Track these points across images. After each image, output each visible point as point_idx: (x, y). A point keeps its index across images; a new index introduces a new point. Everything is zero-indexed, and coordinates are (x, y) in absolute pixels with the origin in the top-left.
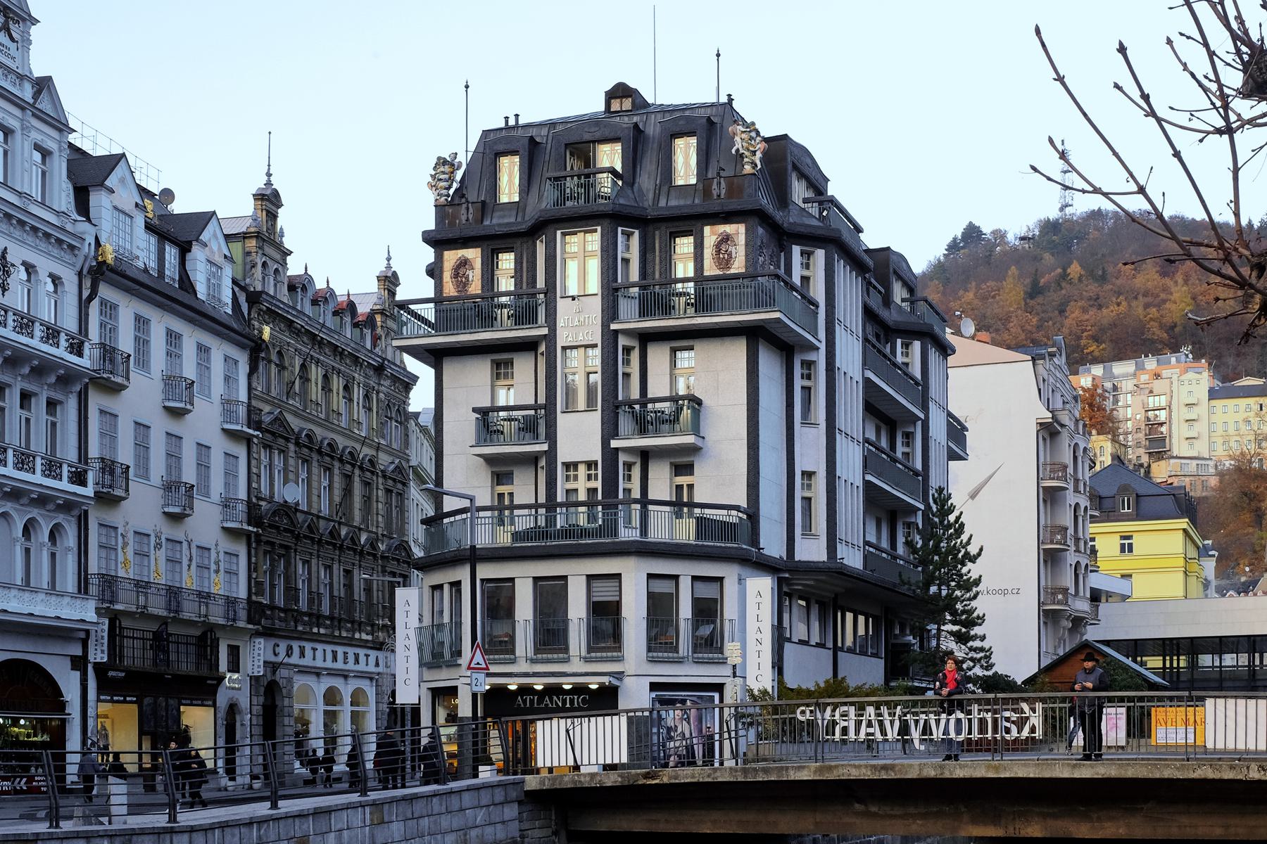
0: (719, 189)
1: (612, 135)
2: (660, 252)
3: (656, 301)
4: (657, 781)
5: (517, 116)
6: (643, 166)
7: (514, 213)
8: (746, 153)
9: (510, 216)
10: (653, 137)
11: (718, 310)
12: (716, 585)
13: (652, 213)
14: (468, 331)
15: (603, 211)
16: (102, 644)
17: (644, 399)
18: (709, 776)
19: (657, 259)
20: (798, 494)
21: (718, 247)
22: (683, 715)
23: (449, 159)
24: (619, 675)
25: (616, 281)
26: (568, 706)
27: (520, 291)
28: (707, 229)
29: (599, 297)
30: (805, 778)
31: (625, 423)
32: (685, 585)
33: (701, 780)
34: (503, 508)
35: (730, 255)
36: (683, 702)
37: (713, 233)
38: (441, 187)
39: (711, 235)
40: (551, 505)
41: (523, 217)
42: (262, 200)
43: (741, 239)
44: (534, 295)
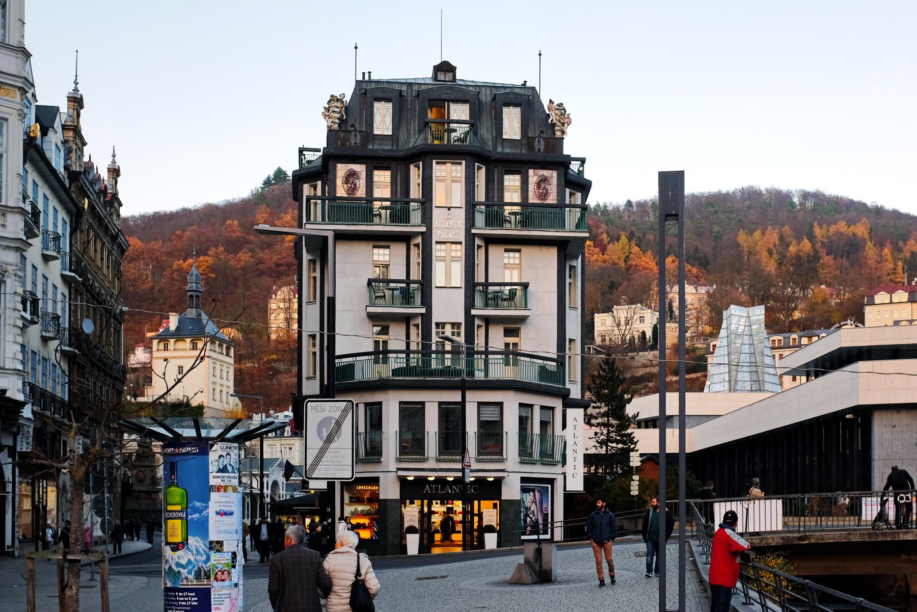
1: (463, 98)
3: (495, 218)
4: (807, 542)
5: (370, 73)
6: (482, 122)
7: (390, 143)
8: (558, 124)
9: (387, 145)
10: (486, 103)
13: (494, 156)
14: (365, 223)
16: (28, 438)
18: (845, 538)
19: (496, 187)
21: (539, 184)
28: (531, 172)
29: (463, 211)
30: (911, 539)
31: (478, 301)
32: (537, 410)
33: (840, 541)
34: (381, 353)
35: (547, 191)
36: (533, 491)
38: (335, 118)
39: (533, 176)
40: (426, 350)
41: (397, 146)
42: (74, 101)
43: (554, 181)
44: (408, 203)
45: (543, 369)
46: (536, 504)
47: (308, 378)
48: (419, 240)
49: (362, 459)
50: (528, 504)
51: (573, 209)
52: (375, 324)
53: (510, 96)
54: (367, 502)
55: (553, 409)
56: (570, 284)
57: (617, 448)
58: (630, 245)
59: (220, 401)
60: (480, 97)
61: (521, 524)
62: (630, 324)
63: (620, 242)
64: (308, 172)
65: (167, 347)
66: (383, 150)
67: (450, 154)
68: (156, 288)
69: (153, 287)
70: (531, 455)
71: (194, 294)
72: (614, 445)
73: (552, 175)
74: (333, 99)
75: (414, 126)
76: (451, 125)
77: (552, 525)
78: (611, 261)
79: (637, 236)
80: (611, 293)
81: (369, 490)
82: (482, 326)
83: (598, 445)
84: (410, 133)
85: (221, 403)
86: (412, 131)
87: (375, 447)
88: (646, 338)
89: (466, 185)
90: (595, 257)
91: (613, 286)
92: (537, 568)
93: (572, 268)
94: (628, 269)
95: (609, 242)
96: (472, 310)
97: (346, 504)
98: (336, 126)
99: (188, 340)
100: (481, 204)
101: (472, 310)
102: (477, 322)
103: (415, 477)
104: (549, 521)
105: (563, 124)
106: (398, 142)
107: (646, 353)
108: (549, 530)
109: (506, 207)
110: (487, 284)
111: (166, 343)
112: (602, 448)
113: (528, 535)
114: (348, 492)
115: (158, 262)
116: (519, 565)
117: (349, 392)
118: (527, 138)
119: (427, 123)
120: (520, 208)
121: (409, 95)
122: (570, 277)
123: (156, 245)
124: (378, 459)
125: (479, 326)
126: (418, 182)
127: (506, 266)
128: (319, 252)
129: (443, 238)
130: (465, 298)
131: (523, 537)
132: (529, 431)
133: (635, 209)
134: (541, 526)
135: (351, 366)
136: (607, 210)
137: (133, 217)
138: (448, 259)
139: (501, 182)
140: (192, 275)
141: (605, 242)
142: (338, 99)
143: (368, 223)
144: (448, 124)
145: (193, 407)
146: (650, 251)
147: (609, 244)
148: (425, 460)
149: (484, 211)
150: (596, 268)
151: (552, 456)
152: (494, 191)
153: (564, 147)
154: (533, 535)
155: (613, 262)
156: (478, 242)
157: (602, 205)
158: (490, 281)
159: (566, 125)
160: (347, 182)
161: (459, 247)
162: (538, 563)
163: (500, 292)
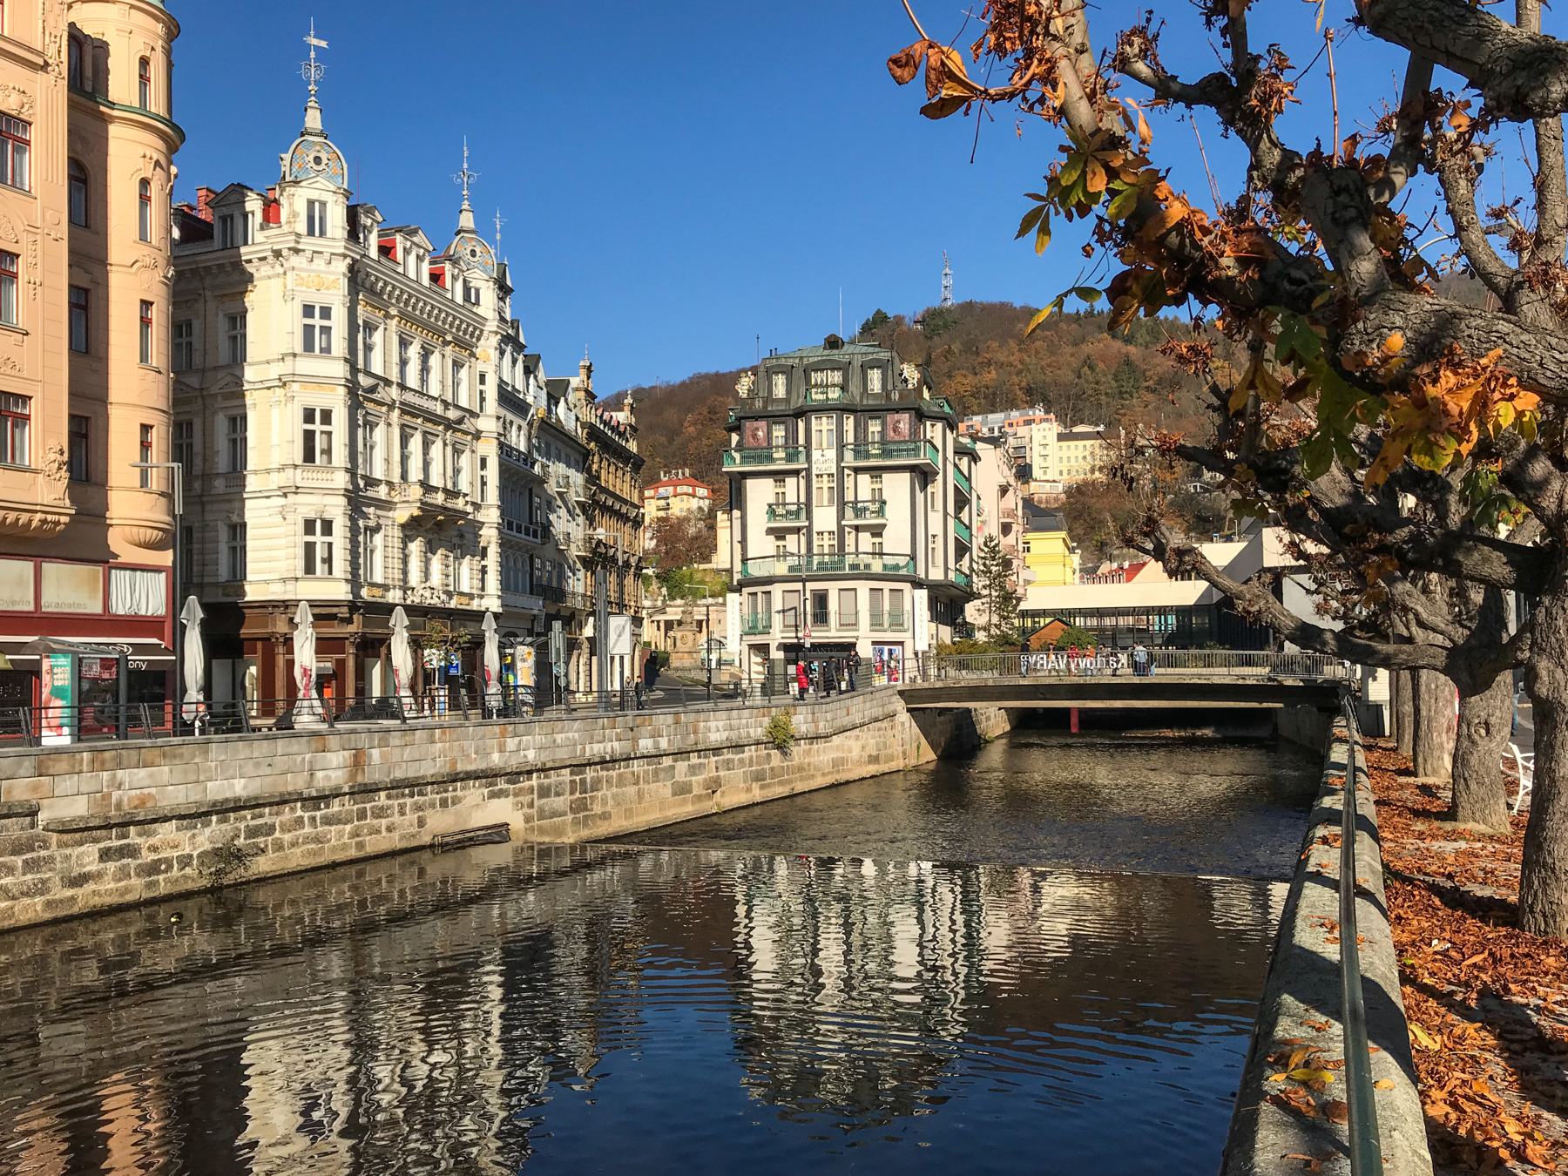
0: (896, 396)
17: (856, 502)
20: (930, 546)
24: (857, 638)
31: (849, 512)
32: (886, 593)
34: (782, 555)
67: (823, 409)
80: (1223, 397)
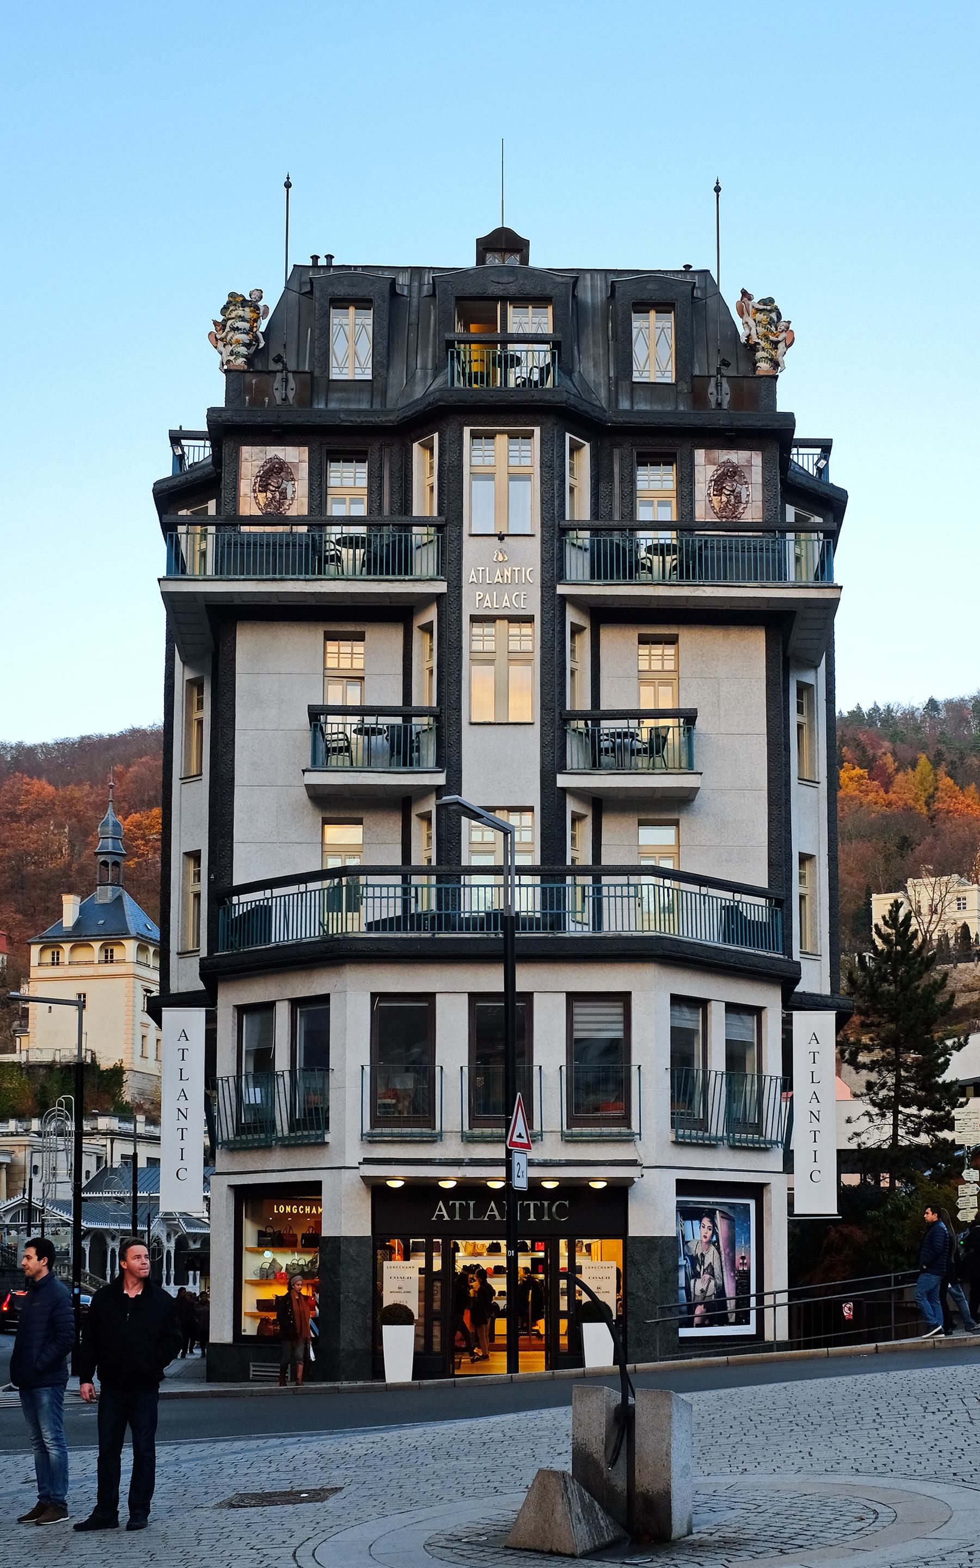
1: (537, 292)
2: (621, 482)
6: (582, 348)
8: (763, 344)
9: (359, 401)
11: (713, 578)
12: (752, 1021)
13: (611, 418)
14: (302, 577)
15: (550, 402)
19: (617, 491)
21: (718, 484)
22: (712, 1237)
23: (248, 298)
25: (564, 518)
26: (532, 1218)
27: (376, 519)
28: (700, 455)
29: (537, 541)
31: (575, 753)
32: (717, 1014)
36: (711, 1214)
37: (710, 461)
38: (238, 342)
41: (384, 403)
43: (756, 475)
44: (407, 527)
45: (732, 913)
46: (718, 1249)
47: (182, 954)
48: (431, 615)
49: (283, 1138)
50: (696, 1248)
51: (803, 536)
52: (328, 815)
53: (650, 286)
54: (303, 1246)
55: (757, 1011)
56: (800, 727)
57: (919, 1117)
58: (936, 775)
59: (156, 1060)
60: (580, 294)
61: (677, 1300)
62: (939, 911)
63: (918, 769)
64: (187, 481)
65: (58, 959)
66: (350, 412)
68: (75, 866)
69: (69, 865)
70: (703, 1124)
71: (109, 859)
72: (913, 1110)
73: (749, 461)
74: (235, 300)
75: (425, 358)
76: (510, 347)
77: (760, 1301)
78: (900, 803)
79: (949, 760)
80: (902, 857)
81: (305, 1215)
82: (585, 816)
83: (874, 1111)
84: (414, 375)
85: (158, 1064)
86: (419, 372)
87: (317, 1109)
88: (970, 938)
89: (542, 483)
90: (871, 796)
91: (905, 844)
92: (620, 1483)
93: (804, 689)
94: (932, 819)
95: (897, 770)
96: (559, 777)
97: (248, 1250)
98: (241, 361)
99: (97, 945)
100: (582, 527)
101: (559, 777)
102: (572, 806)
103: (406, 1179)
104: (753, 1290)
105: (775, 345)
106: (384, 393)
107: (971, 965)
108: (753, 1314)
109: (641, 534)
110: (596, 715)
111: (56, 950)
112: (883, 1116)
113: (698, 1326)
114: (255, 1218)
115: (79, 821)
116: (545, 1475)
117: (254, 976)
118: (688, 380)
119: (450, 344)
120: (673, 534)
121: (415, 294)
122: (800, 710)
123: (73, 791)
124: (318, 1137)
125: (577, 818)
126: (428, 482)
127: (644, 675)
128: (209, 664)
129: (489, 606)
130: (543, 746)
131: (684, 1332)
132: (698, 1064)
133: (943, 715)
134: (731, 1305)
135: (262, 913)
136: (893, 717)
137: (44, 745)
138: (501, 658)
139: (630, 482)
140: (106, 824)
141: (890, 771)
142: (244, 300)
143: (308, 577)
144: (504, 343)
145: (104, 1071)
146: (974, 785)
147: (897, 774)
148: (434, 1139)
149: (587, 543)
150: (873, 815)
151: (758, 1128)
152: (611, 500)
153: (778, 397)
154: (710, 1325)
155: (906, 804)
156: (572, 616)
157: (882, 708)
158: (604, 706)
159: (781, 346)
160: (264, 488)
161: (526, 629)
162: (622, 1463)
163: (626, 735)
